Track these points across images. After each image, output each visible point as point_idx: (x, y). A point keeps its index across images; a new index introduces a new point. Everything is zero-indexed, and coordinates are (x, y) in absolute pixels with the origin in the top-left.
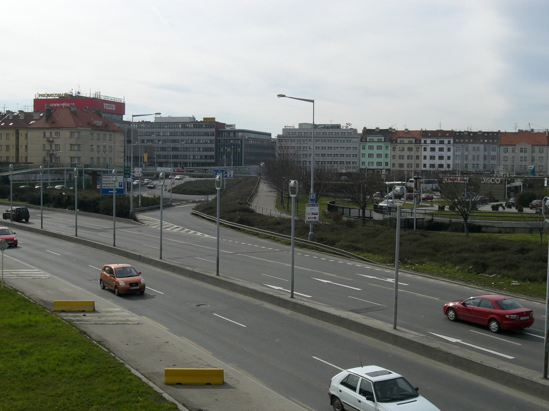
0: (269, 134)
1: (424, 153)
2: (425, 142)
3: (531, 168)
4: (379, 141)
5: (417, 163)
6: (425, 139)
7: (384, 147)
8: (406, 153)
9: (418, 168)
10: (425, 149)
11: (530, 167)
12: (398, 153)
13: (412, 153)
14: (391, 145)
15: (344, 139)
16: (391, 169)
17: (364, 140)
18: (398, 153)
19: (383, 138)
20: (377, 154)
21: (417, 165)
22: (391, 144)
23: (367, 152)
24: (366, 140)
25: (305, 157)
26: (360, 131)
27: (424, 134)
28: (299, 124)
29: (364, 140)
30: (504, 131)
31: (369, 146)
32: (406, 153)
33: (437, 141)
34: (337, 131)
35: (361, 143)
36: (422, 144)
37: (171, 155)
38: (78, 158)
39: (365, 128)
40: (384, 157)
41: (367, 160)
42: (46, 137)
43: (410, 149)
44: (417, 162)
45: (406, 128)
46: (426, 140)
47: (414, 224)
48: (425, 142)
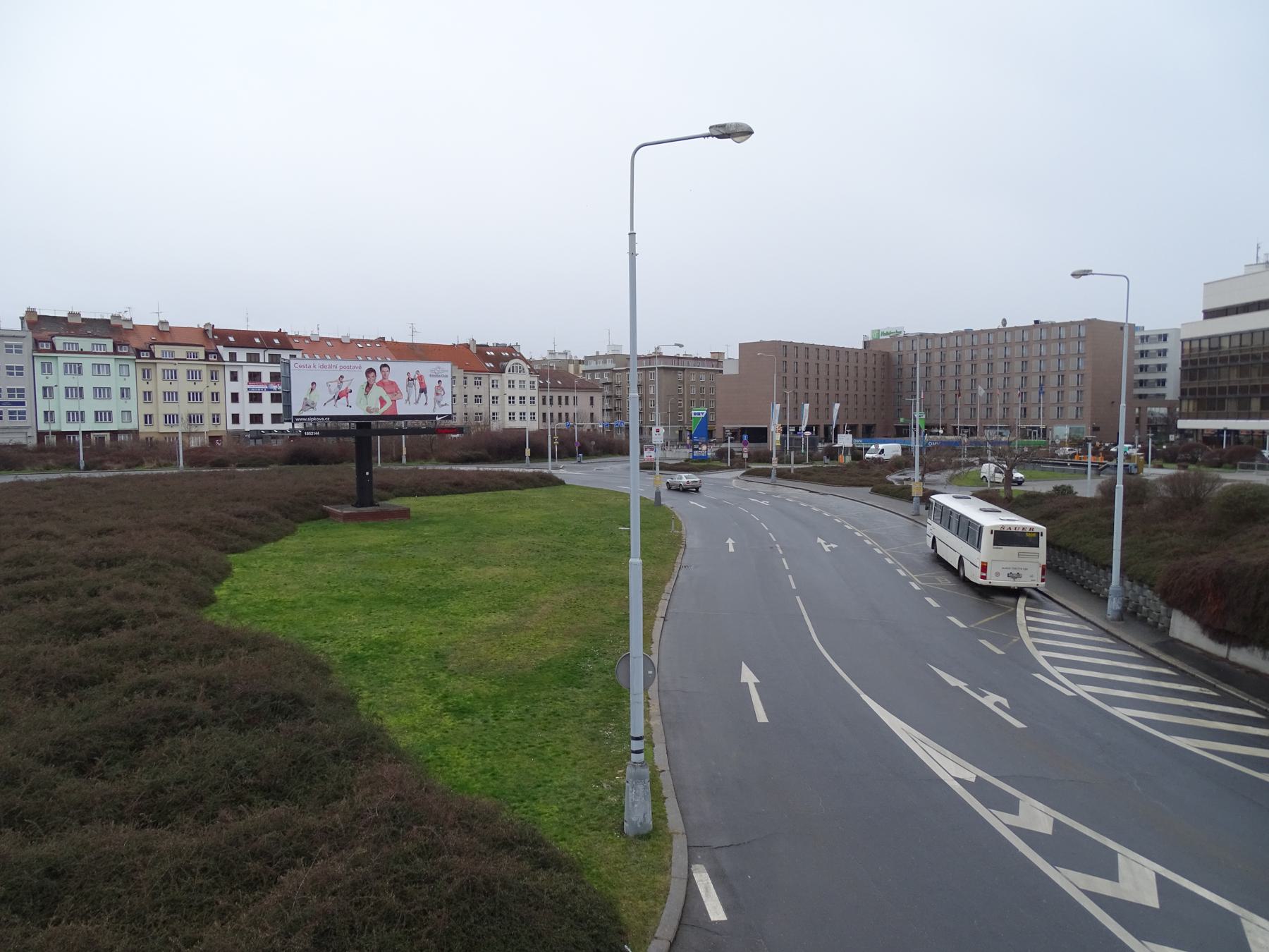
2: (233, 357)
3: (699, 414)
4: (192, 357)
5: (214, 412)
6: (233, 350)
7: (206, 374)
8: (184, 386)
10: (234, 377)
11: (695, 414)
12: (161, 385)
13: (198, 388)
16: (140, 431)
17: (45, 348)
18: (161, 385)
19: (109, 344)
21: (216, 419)
22: (137, 361)
24: (53, 346)
29: (45, 346)
31: (65, 364)
32: (184, 386)
38: (1144, 620)
41: (62, 405)
43: (194, 376)
45: (162, 319)
47: (625, 584)
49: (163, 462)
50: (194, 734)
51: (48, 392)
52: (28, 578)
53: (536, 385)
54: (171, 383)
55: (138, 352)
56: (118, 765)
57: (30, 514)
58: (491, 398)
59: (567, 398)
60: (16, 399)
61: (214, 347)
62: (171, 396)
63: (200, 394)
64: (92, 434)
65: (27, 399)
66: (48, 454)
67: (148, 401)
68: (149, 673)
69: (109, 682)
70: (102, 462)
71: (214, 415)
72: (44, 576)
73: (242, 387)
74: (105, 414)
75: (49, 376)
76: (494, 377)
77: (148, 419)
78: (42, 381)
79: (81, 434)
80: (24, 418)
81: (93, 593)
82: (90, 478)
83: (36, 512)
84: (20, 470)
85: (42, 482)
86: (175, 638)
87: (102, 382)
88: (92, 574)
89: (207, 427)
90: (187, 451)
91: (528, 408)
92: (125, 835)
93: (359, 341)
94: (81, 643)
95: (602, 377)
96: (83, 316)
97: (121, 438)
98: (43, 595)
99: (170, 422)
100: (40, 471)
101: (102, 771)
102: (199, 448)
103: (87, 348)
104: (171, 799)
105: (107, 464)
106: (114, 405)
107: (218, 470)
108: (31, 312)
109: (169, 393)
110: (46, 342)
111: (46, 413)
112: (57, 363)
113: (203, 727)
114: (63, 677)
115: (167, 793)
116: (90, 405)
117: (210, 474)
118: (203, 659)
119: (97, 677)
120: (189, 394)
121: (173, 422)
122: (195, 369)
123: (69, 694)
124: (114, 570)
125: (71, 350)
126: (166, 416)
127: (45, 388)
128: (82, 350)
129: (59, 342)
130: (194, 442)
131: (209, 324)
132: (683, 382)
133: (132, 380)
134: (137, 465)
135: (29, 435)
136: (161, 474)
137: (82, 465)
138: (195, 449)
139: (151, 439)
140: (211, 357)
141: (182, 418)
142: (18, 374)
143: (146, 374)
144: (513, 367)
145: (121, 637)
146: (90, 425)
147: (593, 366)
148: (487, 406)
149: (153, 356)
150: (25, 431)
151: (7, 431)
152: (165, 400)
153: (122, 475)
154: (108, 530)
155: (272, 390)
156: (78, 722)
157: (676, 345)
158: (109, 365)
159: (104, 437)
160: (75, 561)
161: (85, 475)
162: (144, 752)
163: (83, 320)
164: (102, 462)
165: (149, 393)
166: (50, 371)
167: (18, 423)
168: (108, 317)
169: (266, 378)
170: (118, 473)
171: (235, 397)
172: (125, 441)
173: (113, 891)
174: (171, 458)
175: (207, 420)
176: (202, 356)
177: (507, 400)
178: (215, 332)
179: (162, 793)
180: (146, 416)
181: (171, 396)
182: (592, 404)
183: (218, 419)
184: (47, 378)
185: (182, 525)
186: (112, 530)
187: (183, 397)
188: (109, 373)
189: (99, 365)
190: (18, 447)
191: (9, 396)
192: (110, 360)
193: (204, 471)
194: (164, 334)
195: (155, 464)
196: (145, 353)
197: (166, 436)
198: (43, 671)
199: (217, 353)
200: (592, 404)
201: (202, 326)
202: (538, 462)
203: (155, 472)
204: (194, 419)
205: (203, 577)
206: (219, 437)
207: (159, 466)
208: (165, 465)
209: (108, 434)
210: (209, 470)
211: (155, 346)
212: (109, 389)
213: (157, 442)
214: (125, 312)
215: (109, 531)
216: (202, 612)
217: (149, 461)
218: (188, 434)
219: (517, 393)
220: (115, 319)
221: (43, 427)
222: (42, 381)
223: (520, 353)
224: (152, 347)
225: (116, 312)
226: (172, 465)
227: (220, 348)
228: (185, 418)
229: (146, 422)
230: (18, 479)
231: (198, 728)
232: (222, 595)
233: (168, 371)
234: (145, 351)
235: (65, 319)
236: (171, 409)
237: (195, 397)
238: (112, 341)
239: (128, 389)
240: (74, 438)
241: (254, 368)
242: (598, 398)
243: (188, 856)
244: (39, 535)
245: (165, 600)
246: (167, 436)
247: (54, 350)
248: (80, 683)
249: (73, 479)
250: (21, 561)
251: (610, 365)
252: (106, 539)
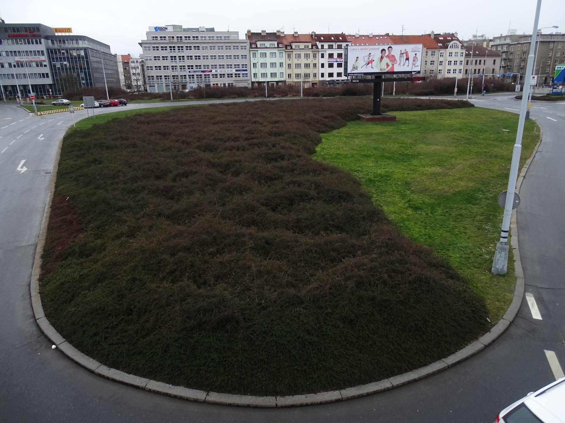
1: (322, 61)
2: (322, 46)
3: (560, 68)
9: (256, 79)
10: (323, 56)
11: (558, 68)
19: (276, 43)
20: (271, 63)
22: (286, 50)
23: (259, 60)
25: (183, 70)
26: (242, 37)
31: (261, 53)
33: (335, 45)
35: (250, 50)
36: (320, 50)
39: (249, 31)
41: (259, 70)
42: (291, 44)
43: (307, 56)
44: (315, 71)
45: (295, 31)
48: (322, 46)
53: (464, 55)
58: (439, 62)
59: (480, 61)
73: (326, 61)
76: (442, 51)
91: (458, 67)
93: (377, 36)
95: (502, 48)
132: (552, 49)
144: (452, 45)
147: (498, 42)
148: (437, 66)
155: (338, 61)
157: (554, 27)
163: (267, 33)
169: (335, 56)
171: (323, 66)
177: (447, 63)
182: (494, 63)
200: (494, 63)
219: (453, 59)
221: (253, 80)
223: (457, 37)
241: (331, 51)
242: (498, 60)
251: (508, 41)
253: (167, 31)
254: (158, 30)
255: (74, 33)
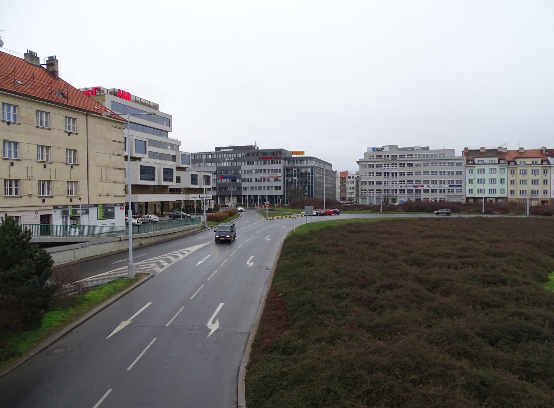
0: (138, 158)
8: (530, 177)
13: (537, 177)
14: (508, 167)
15: (461, 161)
16: (508, 198)
17: (471, 163)
18: (519, 177)
19: (496, 160)
22: (509, 166)
24: (474, 162)
26: (459, 153)
27: (547, 153)
28: (216, 148)
29: (471, 162)
30: (537, 149)
31: (478, 169)
34: (426, 152)
35: (467, 166)
37: (259, 190)
40: (517, 181)
41: (476, 186)
43: (535, 172)
45: (521, 147)
46: (13, 162)
49: (518, 212)
50: (544, 343)
51: (471, 181)
52: (466, 257)
54: (523, 176)
55: (509, 163)
56: (508, 346)
57: (465, 231)
60: (459, 184)
61: (546, 158)
62: (524, 182)
63: (538, 180)
64: (487, 199)
65: (463, 184)
66: (470, 206)
67: (512, 184)
68: (520, 308)
69: (502, 308)
70: (491, 211)
71: (544, 191)
72: (473, 257)
74: (493, 190)
75: (471, 174)
77: (512, 192)
78: (469, 176)
79: (483, 198)
80: (461, 192)
81: (493, 267)
82: (487, 217)
83: (468, 230)
84: (460, 213)
85: (469, 218)
86: (531, 295)
87: (493, 176)
88: (491, 259)
89: (541, 196)
90: (531, 207)
92: (513, 380)
94: (489, 288)
96: (486, 148)
97: (500, 200)
98: (473, 265)
99: (522, 194)
100: (467, 214)
101: (501, 347)
102: (536, 206)
103: (487, 162)
104: (534, 371)
105: (494, 212)
106: (497, 186)
107: (547, 217)
108: (466, 149)
109: (522, 180)
110: (471, 160)
111: (470, 190)
112: (475, 169)
113: (549, 341)
114: (482, 301)
115: (532, 367)
116: (487, 186)
117: (543, 219)
118: (547, 308)
119: (496, 304)
120: (532, 181)
121: (524, 194)
122: (523, 169)
123: (486, 309)
124: (501, 259)
125: (481, 163)
126: (520, 191)
127: (470, 180)
128: (485, 163)
129: (476, 160)
130: (534, 204)
131: (543, 147)
133: (506, 175)
134: (507, 213)
135: (463, 198)
136: (545, 218)
137: (483, 212)
138: (534, 207)
139: (513, 201)
140: (544, 163)
141: (529, 192)
142: (452, 174)
143: (512, 172)
145: (507, 289)
146: (487, 195)
149: (516, 164)
150: (461, 197)
151: (455, 197)
152: (520, 184)
153: (501, 217)
154: (497, 241)
156: (490, 322)
158: (496, 169)
159: (492, 200)
160: (484, 252)
161: (485, 216)
162: (519, 344)
164: (491, 211)
165: (513, 180)
166: (472, 172)
167: (459, 194)
168: (496, 148)
170: (499, 216)
172: (501, 202)
173: (509, 403)
174: (523, 210)
175: (541, 193)
176: (539, 162)
178: (547, 150)
179: (529, 366)
180: (511, 191)
181: (524, 182)
183: (546, 193)
184: (471, 175)
185: (531, 242)
186: (499, 241)
187: (529, 182)
188: (496, 172)
189: (492, 169)
190: (459, 203)
191: (457, 183)
192: (497, 167)
193: (540, 217)
194: (522, 154)
195: (515, 213)
196: (471, 161)
197: (519, 200)
198: (475, 297)
199: (548, 161)
201: (540, 148)
202: (406, 218)
203: (516, 216)
204: (534, 192)
205: (542, 268)
206: (547, 201)
207: (517, 214)
208: (520, 214)
209: (494, 199)
210: (542, 217)
211: (517, 159)
212: (495, 179)
213: (516, 203)
214: (504, 145)
215: (497, 241)
216: (542, 285)
217: (513, 212)
218: (531, 200)
220: (482, 149)
222: (469, 176)
224: (515, 160)
225: (500, 145)
226: (523, 213)
227: (549, 158)
228: (530, 192)
229: (511, 194)
230: (459, 216)
231: (546, 341)
232: (552, 278)
233: (522, 170)
234: (512, 162)
235: (479, 150)
236: (523, 187)
237: (535, 182)
238: (498, 158)
239: (504, 179)
240: (480, 200)
243: (545, 402)
244: (469, 240)
245: (525, 276)
246: (521, 200)
247: (474, 164)
248: (489, 306)
249: (481, 217)
250: (463, 249)
252: (497, 244)
253: (383, 150)
254: (375, 150)
255: (306, 155)
